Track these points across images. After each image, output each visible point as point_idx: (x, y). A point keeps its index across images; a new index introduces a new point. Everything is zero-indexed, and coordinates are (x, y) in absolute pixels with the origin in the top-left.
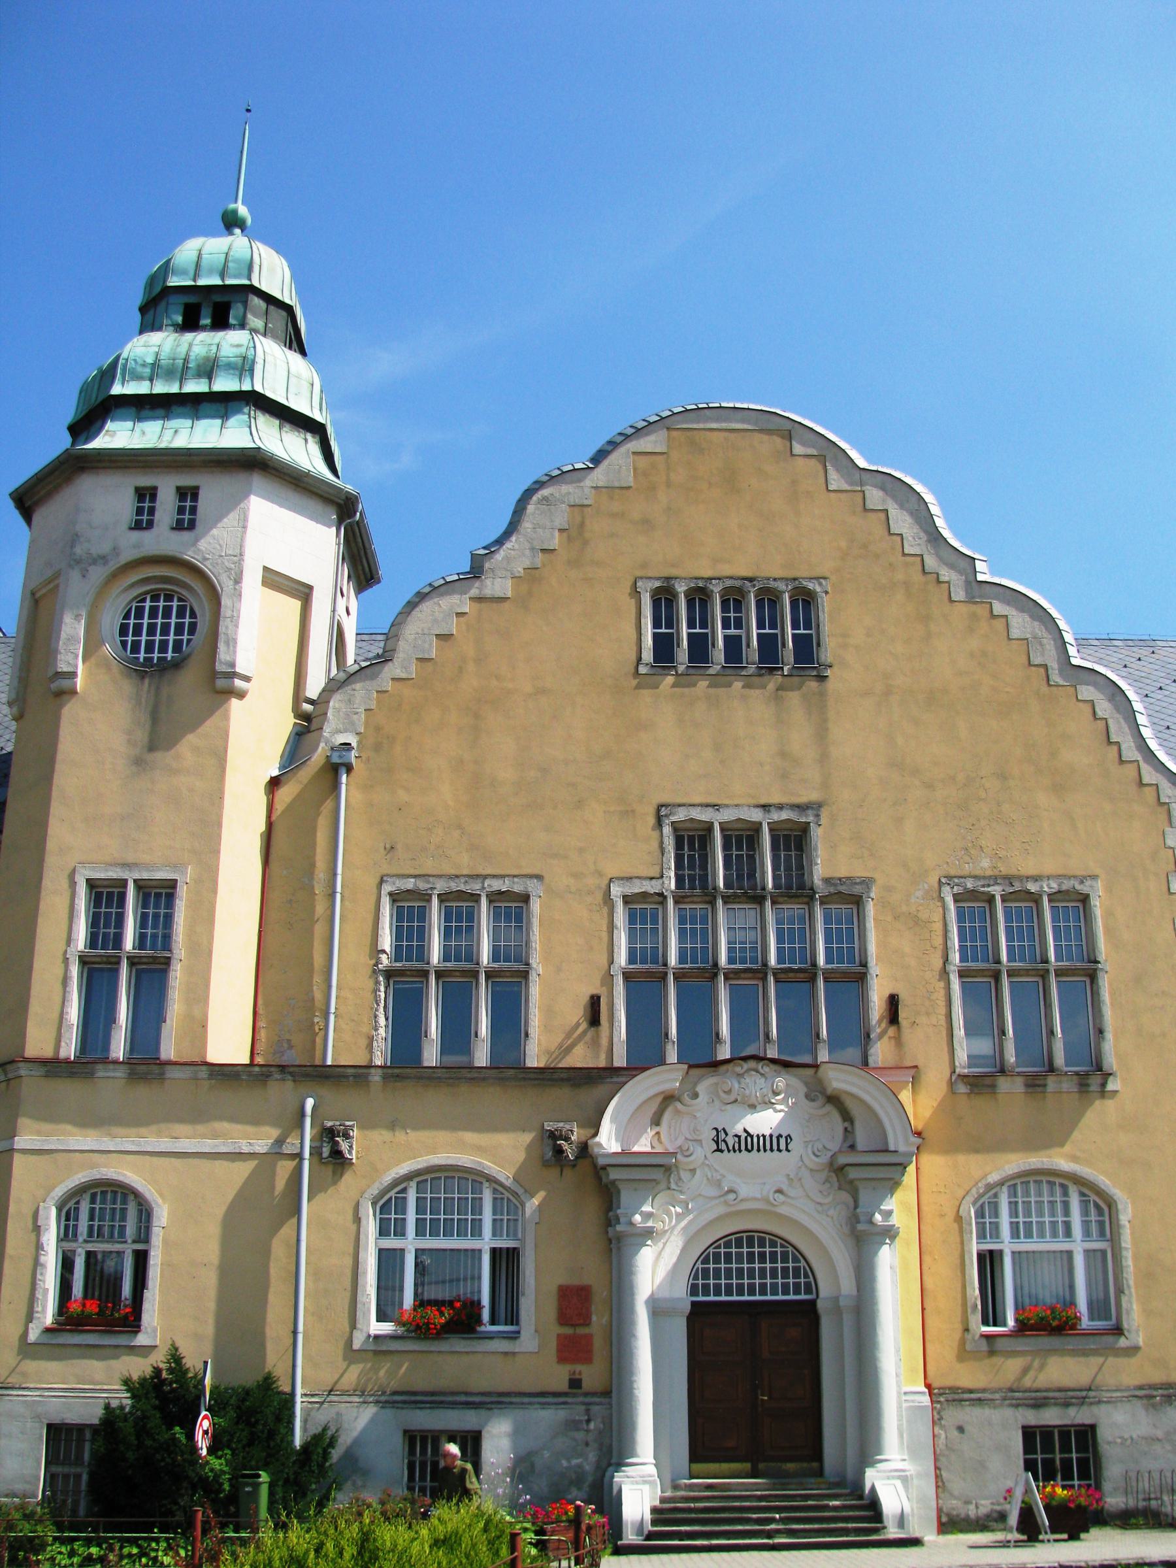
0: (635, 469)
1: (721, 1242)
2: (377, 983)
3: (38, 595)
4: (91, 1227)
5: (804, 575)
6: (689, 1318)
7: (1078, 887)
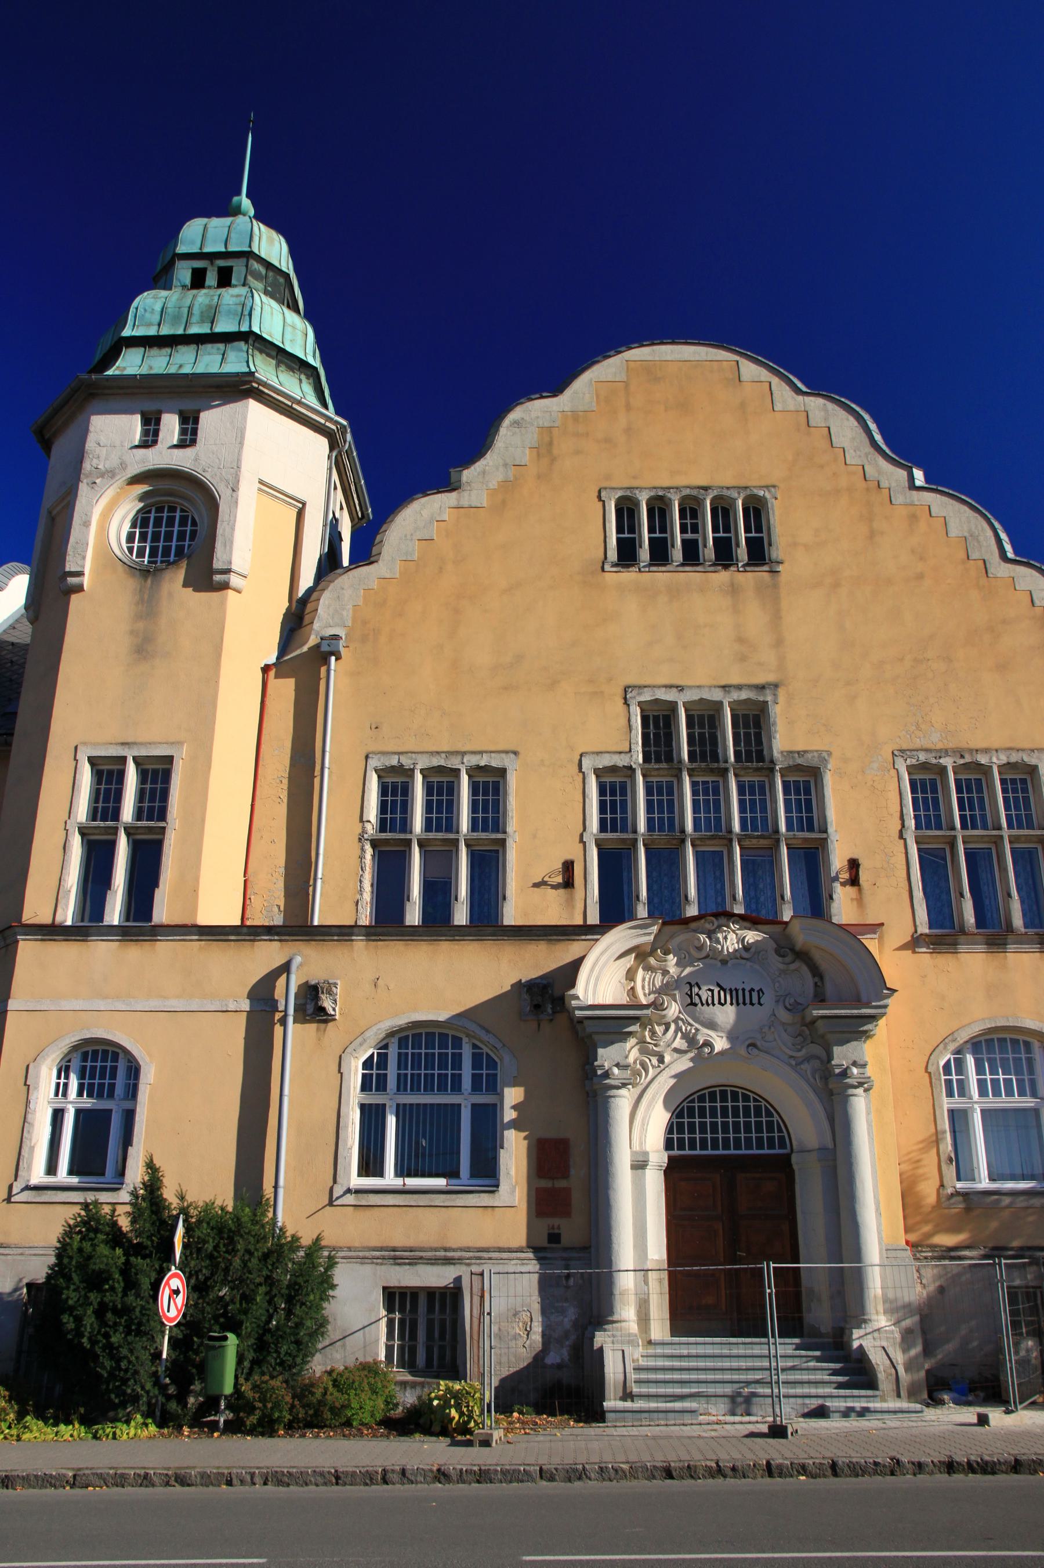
0: (597, 396)
1: (695, 1096)
2: (363, 850)
5: (754, 484)
6: (665, 1171)
7: (1026, 759)
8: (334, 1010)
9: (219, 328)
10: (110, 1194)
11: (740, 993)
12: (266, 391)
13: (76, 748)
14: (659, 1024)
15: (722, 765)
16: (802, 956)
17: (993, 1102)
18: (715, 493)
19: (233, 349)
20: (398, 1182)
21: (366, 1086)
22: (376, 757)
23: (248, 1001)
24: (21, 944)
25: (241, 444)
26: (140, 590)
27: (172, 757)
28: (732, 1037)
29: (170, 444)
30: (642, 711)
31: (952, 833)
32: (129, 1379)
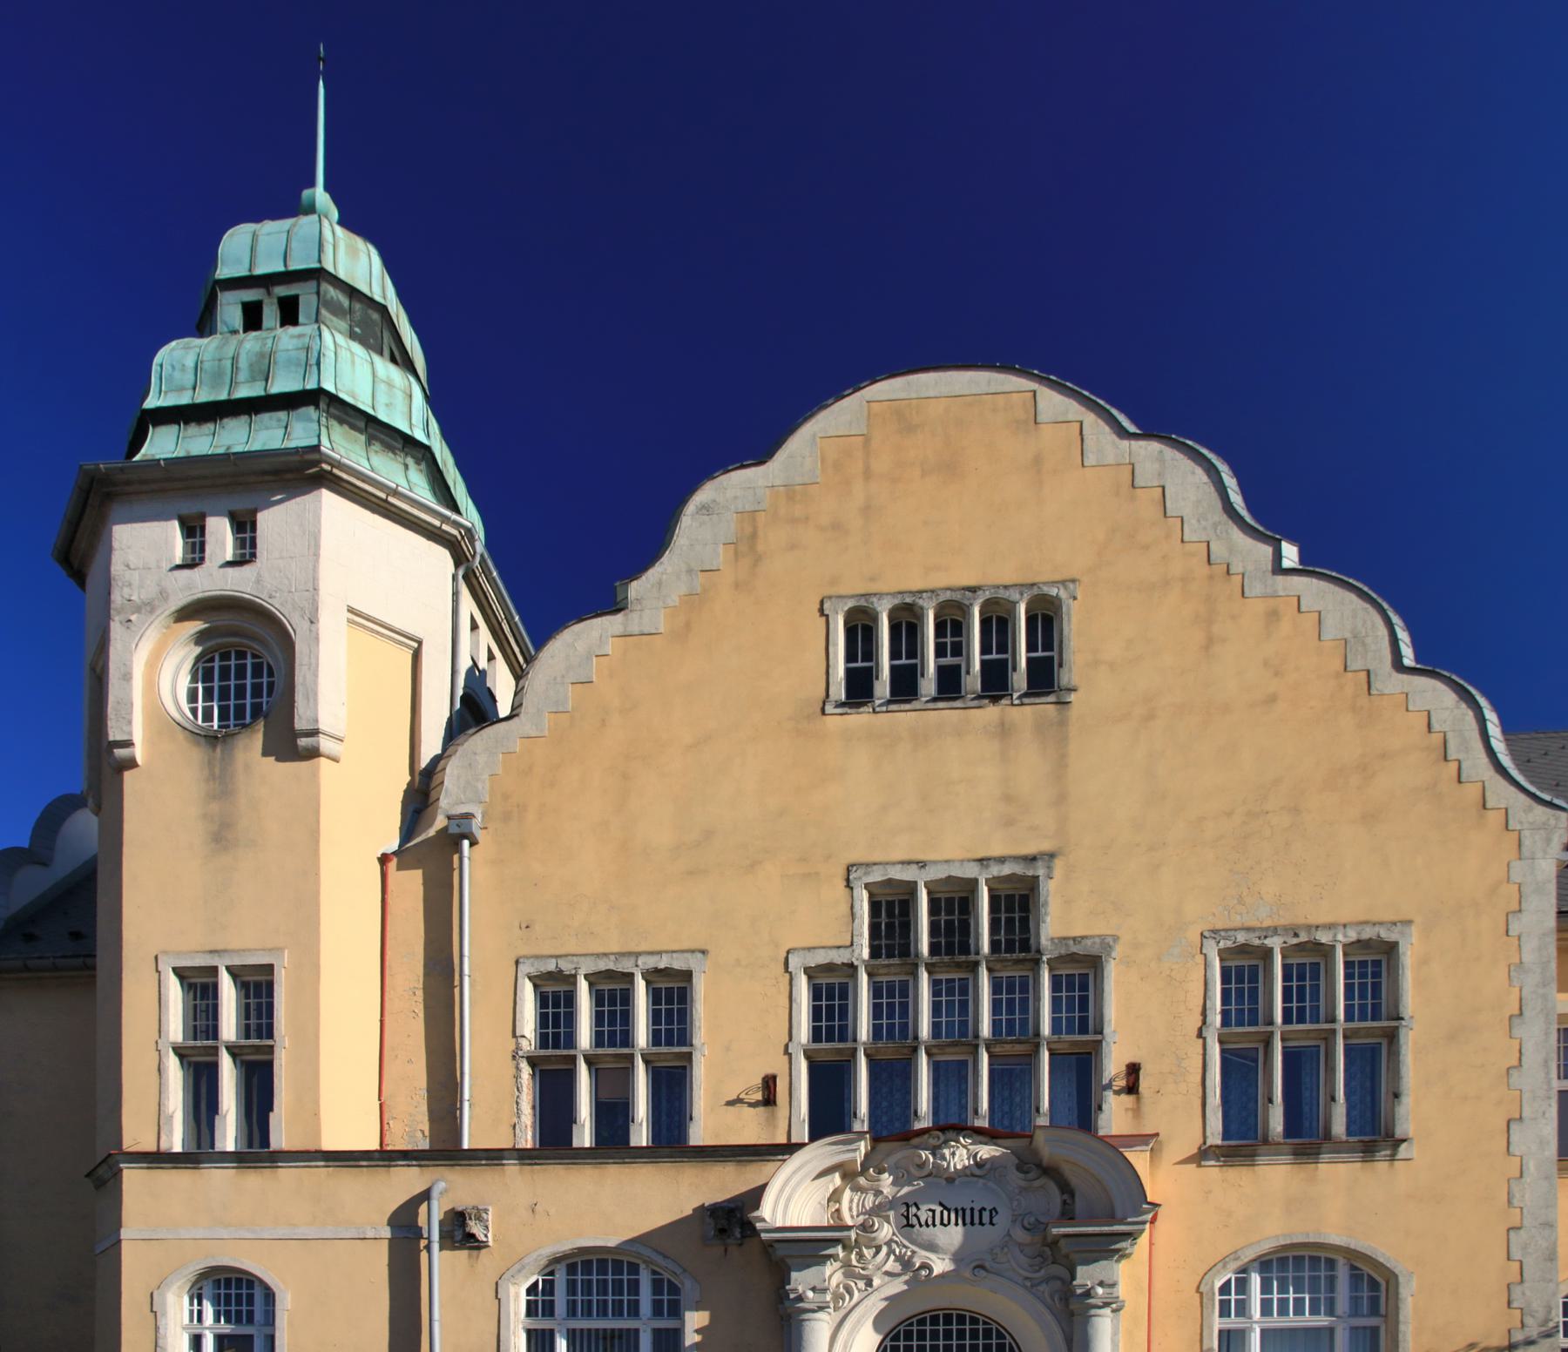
0: (823, 461)
2: (518, 1069)
9: (276, 388)
11: (968, 1213)
12: (345, 476)
14: (868, 1247)
15: (972, 957)
16: (1050, 1171)
17: (1276, 1321)
18: (988, 595)
19: (298, 419)
21: (531, 1310)
22: (528, 962)
23: (388, 1229)
24: (125, 1172)
25: (317, 555)
26: (209, 762)
27: (271, 967)
28: (957, 1258)
29: (222, 562)
30: (871, 895)
31: (1269, 1029)
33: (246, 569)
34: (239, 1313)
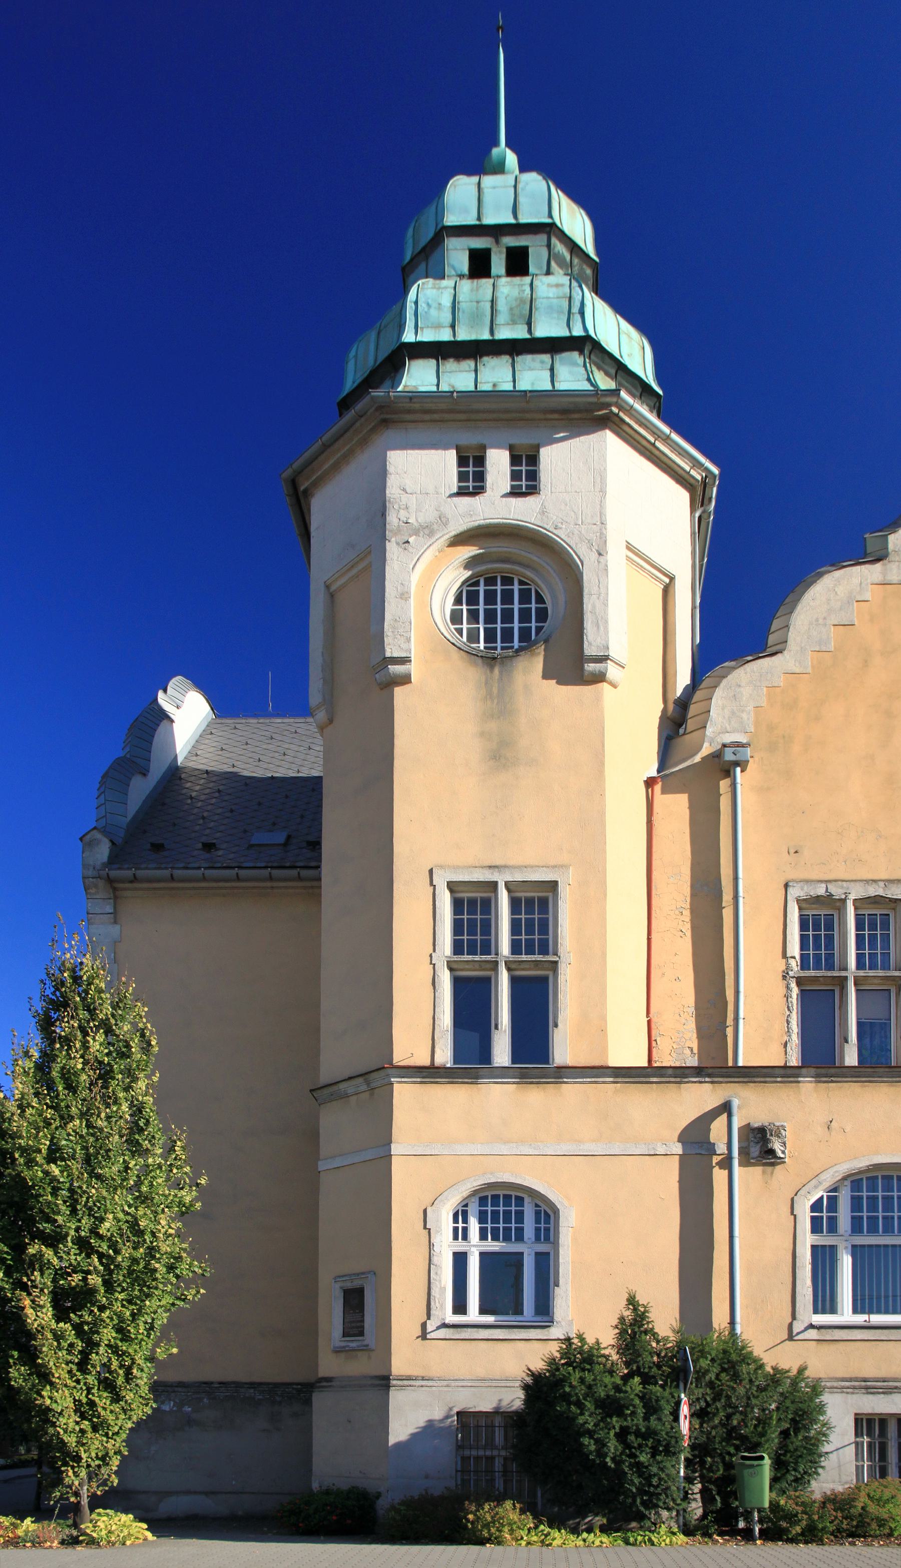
2: (788, 987)
3: (333, 588)
4: (538, 1230)
8: (783, 1152)
10: (538, 1331)
13: (431, 872)
20: (860, 1319)
23: (679, 1145)
24: (395, 1085)
25: (603, 491)
26: (486, 683)
27: (555, 883)
31: (843, 974)
32: (660, 1494)
33: (530, 500)
34: (507, 1230)
